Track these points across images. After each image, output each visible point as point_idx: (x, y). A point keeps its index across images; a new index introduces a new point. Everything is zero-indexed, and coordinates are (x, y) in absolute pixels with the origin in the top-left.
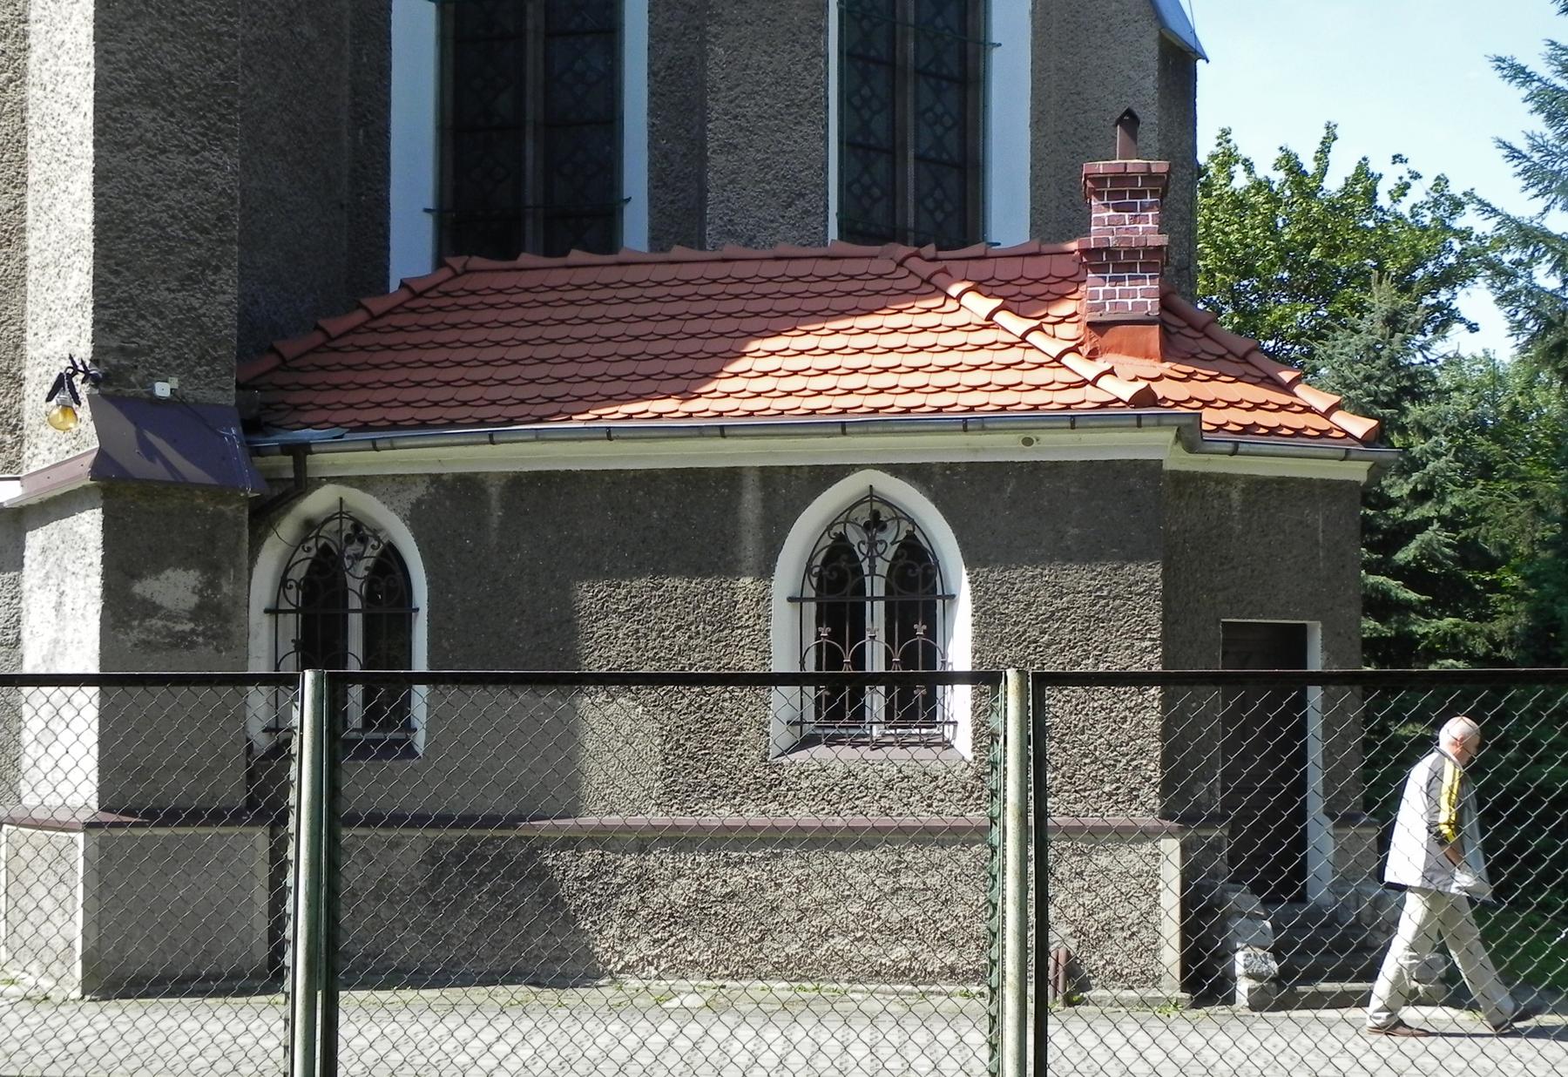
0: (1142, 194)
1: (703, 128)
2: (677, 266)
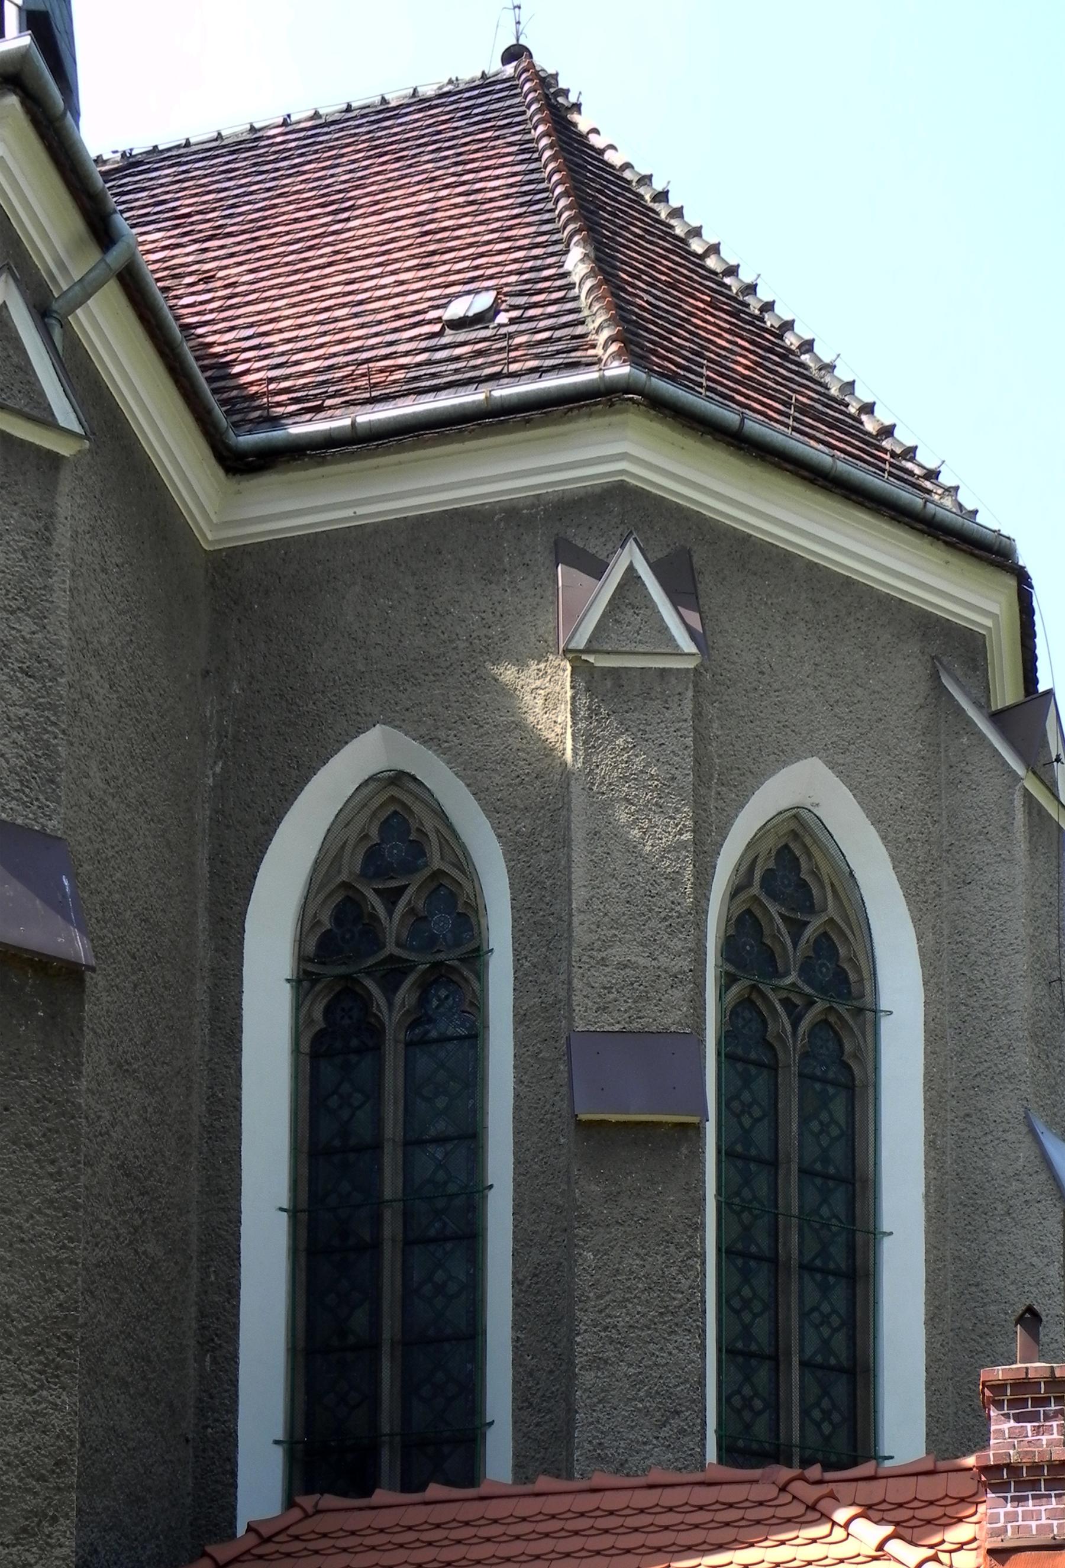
0: (1045, 1401)
1: (571, 1341)
2: (543, 1499)
